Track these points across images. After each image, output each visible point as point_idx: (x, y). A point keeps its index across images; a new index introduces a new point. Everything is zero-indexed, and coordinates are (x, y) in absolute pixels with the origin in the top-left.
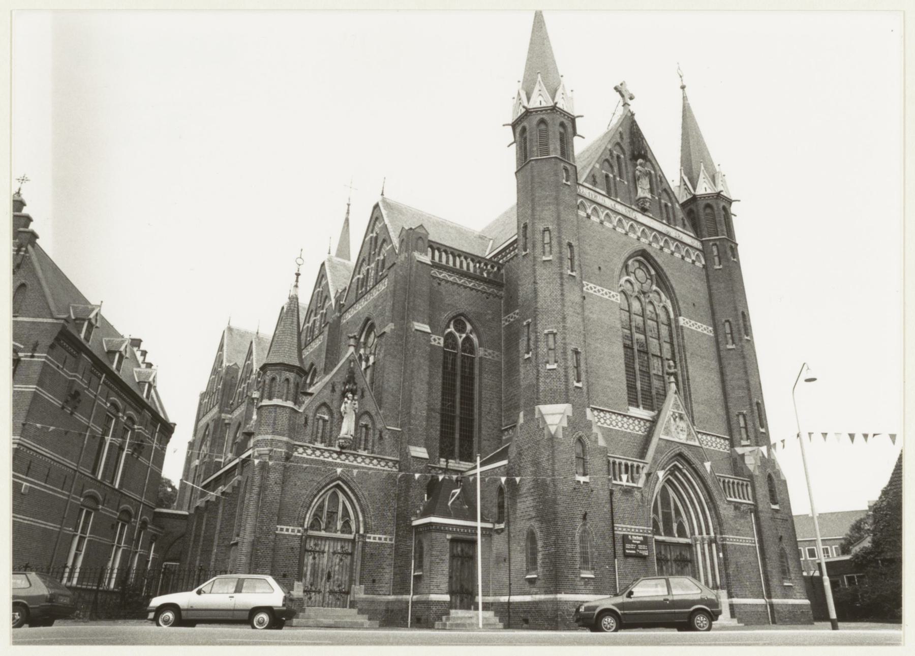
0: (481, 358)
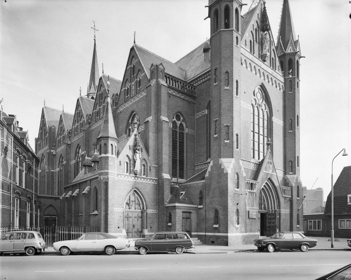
0: (187, 133)
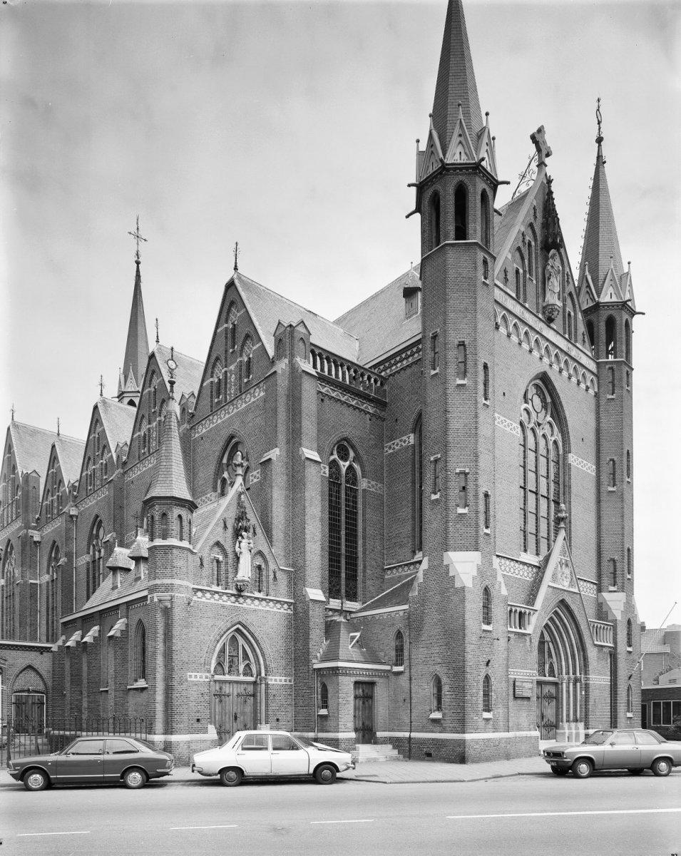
0: (364, 490)
